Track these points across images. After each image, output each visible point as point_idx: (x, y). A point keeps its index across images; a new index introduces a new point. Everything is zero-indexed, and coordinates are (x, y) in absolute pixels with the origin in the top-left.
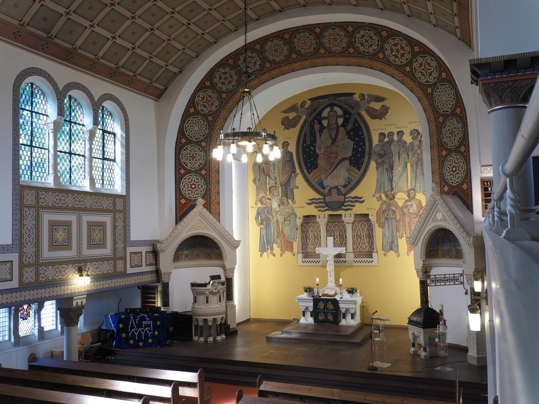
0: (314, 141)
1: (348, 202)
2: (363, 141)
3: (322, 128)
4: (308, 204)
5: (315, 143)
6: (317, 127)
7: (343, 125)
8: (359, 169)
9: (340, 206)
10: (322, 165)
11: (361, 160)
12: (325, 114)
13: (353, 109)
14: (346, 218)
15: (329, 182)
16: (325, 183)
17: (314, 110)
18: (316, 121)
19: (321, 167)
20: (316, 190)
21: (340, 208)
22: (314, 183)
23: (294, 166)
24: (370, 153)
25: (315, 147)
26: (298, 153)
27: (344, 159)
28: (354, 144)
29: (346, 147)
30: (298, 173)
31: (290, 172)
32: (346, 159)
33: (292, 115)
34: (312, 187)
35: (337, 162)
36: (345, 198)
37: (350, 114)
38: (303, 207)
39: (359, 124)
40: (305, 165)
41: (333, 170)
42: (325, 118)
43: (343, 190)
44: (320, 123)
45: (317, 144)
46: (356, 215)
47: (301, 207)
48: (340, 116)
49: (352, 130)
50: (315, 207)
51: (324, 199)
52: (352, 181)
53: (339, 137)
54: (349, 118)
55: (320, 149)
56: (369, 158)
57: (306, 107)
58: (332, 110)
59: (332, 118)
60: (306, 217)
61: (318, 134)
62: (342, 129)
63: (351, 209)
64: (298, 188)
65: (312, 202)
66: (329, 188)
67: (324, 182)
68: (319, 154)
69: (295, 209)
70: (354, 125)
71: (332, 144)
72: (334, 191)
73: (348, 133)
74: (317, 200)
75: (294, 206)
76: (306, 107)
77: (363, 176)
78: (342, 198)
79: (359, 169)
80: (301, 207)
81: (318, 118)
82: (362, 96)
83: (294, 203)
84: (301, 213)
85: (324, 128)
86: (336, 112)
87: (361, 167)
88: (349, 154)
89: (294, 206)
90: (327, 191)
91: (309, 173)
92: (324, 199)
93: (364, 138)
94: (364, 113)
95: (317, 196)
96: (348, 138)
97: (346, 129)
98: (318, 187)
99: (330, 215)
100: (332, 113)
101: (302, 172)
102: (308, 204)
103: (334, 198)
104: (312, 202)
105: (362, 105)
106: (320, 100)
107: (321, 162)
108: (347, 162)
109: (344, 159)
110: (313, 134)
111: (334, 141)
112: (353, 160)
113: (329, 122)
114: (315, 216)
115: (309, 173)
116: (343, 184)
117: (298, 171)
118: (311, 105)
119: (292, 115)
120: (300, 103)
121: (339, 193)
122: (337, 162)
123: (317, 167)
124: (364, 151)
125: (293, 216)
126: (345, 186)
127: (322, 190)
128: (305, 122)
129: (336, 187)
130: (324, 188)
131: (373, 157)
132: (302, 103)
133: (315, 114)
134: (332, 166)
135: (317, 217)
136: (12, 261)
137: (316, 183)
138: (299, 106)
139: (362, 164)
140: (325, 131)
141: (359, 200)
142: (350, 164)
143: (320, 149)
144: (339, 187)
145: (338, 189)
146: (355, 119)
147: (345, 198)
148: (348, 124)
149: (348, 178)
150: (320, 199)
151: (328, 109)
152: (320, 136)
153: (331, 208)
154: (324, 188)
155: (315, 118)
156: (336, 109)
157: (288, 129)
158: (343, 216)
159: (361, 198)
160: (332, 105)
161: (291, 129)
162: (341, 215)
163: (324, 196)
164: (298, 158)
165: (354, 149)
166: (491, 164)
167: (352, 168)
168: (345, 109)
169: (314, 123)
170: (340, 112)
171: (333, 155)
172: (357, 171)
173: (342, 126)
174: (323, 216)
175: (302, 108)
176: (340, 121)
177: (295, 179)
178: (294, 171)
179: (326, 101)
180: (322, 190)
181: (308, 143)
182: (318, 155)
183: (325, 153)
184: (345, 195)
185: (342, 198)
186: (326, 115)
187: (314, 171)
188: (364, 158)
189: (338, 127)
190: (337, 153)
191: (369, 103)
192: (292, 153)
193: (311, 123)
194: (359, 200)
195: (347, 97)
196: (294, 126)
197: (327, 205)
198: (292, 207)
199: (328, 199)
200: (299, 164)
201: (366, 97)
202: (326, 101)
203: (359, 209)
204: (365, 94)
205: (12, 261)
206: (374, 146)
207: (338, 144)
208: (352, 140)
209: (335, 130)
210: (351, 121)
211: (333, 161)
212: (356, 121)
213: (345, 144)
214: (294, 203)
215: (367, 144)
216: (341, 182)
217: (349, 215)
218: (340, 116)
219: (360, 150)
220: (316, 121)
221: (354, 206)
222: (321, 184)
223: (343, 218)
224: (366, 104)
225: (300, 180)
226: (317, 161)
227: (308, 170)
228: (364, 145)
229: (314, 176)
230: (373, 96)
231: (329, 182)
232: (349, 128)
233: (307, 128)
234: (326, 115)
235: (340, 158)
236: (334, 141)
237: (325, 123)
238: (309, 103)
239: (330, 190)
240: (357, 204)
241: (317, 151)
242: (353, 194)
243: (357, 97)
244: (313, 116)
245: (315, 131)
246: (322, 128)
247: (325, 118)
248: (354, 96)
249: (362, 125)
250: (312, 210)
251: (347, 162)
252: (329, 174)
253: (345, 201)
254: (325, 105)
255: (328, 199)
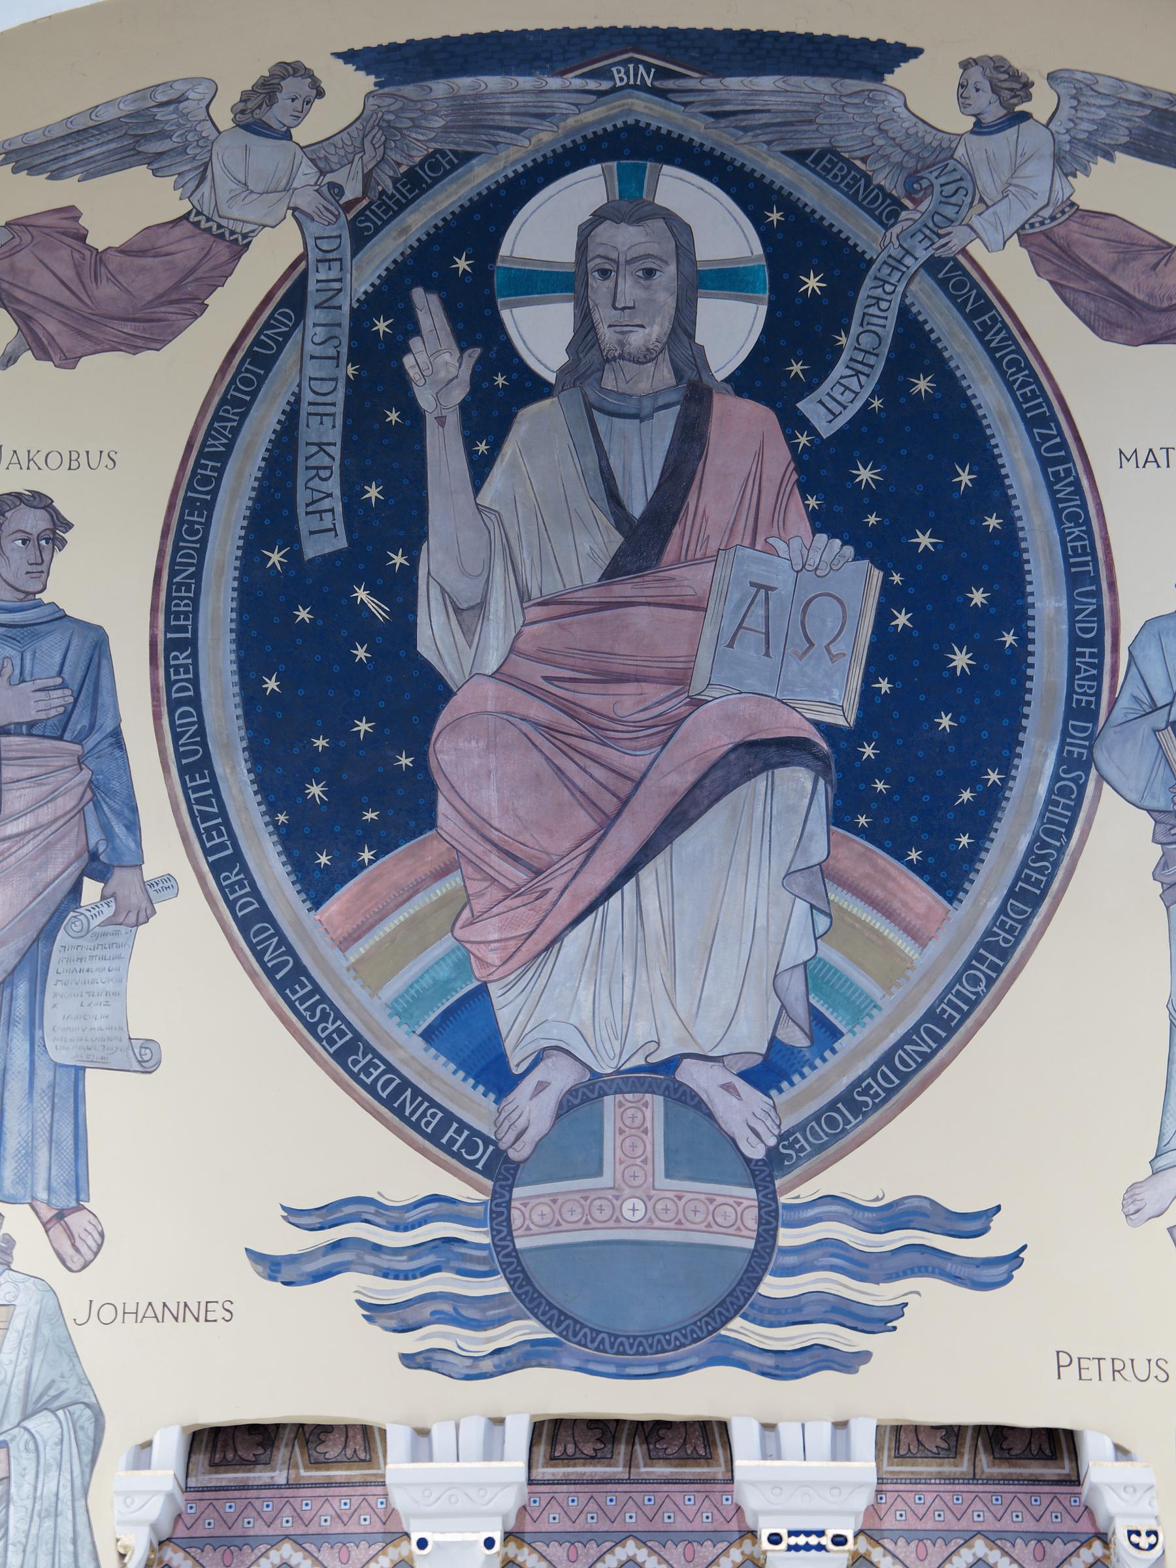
0: (406, 519)
1: (805, 1260)
2: (1005, 564)
3: (501, 393)
4: (273, 1267)
5: (414, 535)
6: (437, 367)
7: (759, 377)
8: (948, 876)
9: (711, 1309)
10: (489, 800)
11: (974, 779)
12: (542, 232)
13: (886, 210)
14: (789, 1466)
15: (573, 1007)
16: (522, 1016)
17: (415, 184)
18: (429, 309)
19: (479, 826)
20: (398, 1101)
21: (697, 1337)
22: (370, 1007)
23: (110, 798)
24: (1082, 713)
25: (401, 591)
26: (175, 644)
27: (763, 754)
28: (889, 599)
29: (792, 620)
30: (168, 884)
31: (61, 863)
32: (788, 749)
33: (124, 206)
34: (349, 1053)
35: (681, 781)
36: (770, 1218)
37: (847, 266)
38: (203, 1314)
39: (950, 384)
40: (264, 786)
41: (630, 871)
42: (538, 283)
43: (748, 1118)
44: (477, 325)
45: (441, 564)
46: (903, 1440)
47: (182, 1312)
48: (728, 280)
49: (861, 435)
50: (373, 1311)
51: (499, 1214)
52: (861, 1008)
53: (713, 501)
54: (837, 308)
55: (469, 615)
56: (1076, 766)
57: (305, 134)
58: (630, 205)
59: (629, 289)
60: (222, 1446)
61: (445, 453)
62: (744, 433)
63: (850, 1362)
64: (145, 1058)
65: (329, 1242)
66: (560, 1077)
67: (508, 1008)
68: (450, 669)
69: (86, 1340)
70: (892, 384)
71: (615, 571)
72: (634, 1129)
73: (820, 470)
74: (399, 1218)
75: (74, 1292)
76: (305, 134)
77: (995, 957)
78: (723, 1215)
79: (948, 876)
80: (182, 1312)
81: (464, 269)
82: (1001, 90)
83: (79, 1254)
84: (161, 1394)
85: (531, 387)
86: (680, 232)
87: (973, 856)
88: (830, 694)
89: (74, 1292)
90: (532, 1111)
91: (317, 889)
92: (499, 1214)
93: (1010, 535)
94: (1012, 273)
95: (403, 1171)
96: (820, 522)
97: (793, 423)
98: (441, 1067)
99: (555, 1436)
100: (624, 238)
101: (225, 864)
102: (273, 1267)
103: (633, 1209)
104: (329, 1242)
105: (987, 184)
106: (493, 83)
107: (474, 765)
108: (798, 785)
109: (763, 754)
110: (381, 433)
111: (645, 539)
112: (874, 769)
113: (585, 328)
114: (364, 1440)
115: (317, 889)
116: (751, 1039)
117: (164, 842)
118: (372, 126)
119: (124, 206)
120: (236, 81)
121: (696, 1143)
122: (674, 776)
123: (425, 819)
124: (1005, 678)
125: (44, 1426)
126: (769, 1071)
127: (472, 1105)
128: (292, 298)
129: (661, 1076)
130: (496, 1076)
131: (1123, 754)
132: (267, 89)
133: (419, 220)
134: (608, 822)
135: (398, 1440)
136: (1169, 1229)
137: (403, 1010)
138: (223, 116)
139: (983, 817)
140: (535, 425)
141: (944, 1243)
142: (840, 817)
143: (469, 615)
144: (693, 1075)
145: (684, 1099)
146: (910, 328)
147: (770, 1218)
148: (820, 369)
149: (814, 973)
150: (436, 1205)
151: (586, 189)
152: (480, 469)
153: (575, 1337)
154: (496, 1076)
155: (422, 265)
156: (678, 190)
157: (69, 361)
158: (745, 1436)
159: (976, 1223)
160: (632, 149)
161: (102, 367)
162: (705, 1439)
163: (502, 1171)
164: (179, 701)
165: (885, 652)
166: (452, 1425)
167: (859, 856)
168: (789, 204)
169: (407, 326)
170: (723, 232)
171: (627, 702)
172: (918, 894)
173: (745, 381)
174: (474, 1430)
175: (263, 147)
176: (730, 330)
177: (121, 955)
178: (106, 859)
179: (572, 102)
180: (472, 1105)
181: (323, 536)
182: (433, 691)
183: (535, 673)
184: (764, 1173)
185: (723, 1215)
186: (564, 253)
187: (383, 873)
188: (1004, 748)
189: (696, 396)
190: (680, 678)
191: (1067, 162)
192: (96, 644)
193: (362, 315)
194: (944, 1243)
195: (822, 85)
196: (150, 324)
197: (529, 1296)
198: (52, 1314)
199: (544, 1216)
200: (193, 766)
201: (1041, 103)
202: (572, 102)
203: (952, 1359)
204: (1031, 62)
205: (1169, 1229)
206: (1126, 639)
207: (693, 579)
208: (867, 547)
209: (666, 424)
210: (867, 335)
211: (633, 763)
212: (913, 345)
213: (781, 578)
214: (79, 1254)
215: (1048, 603)
216: (721, 1010)
217: (821, 1433)
218: (728, 280)
219: (961, 660)
220: (429, 309)
221: (879, 1321)
222: (469, 1032)
223: (747, 1462)
224: (1039, 177)
225: (180, 964)
226: (420, 746)
227: (297, 844)
228: (1013, 607)
229: (383, 936)
230: (1120, 95)
231: (573, 1007)
232: (832, 406)
233: (314, 371)
234: (564, 253)
235: (709, 735)
236: (645, 539)
237: (541, 333)
238: (347, 96)
239: (586, 1095)
240: (927, 1297)
241: (435, 635)
242: (872, 1169)
243: (928, 95)
244: (388, 248)
245: (414, 416)
246: (501, 393)
247: (538, 283)
248: (901, 77)
249: (989, 395)
250: (313, 1357)
251: (798, 785)
252: (568, 907)
253: (763, 1257)
254: (545, 138)
255: (544, 1216)
